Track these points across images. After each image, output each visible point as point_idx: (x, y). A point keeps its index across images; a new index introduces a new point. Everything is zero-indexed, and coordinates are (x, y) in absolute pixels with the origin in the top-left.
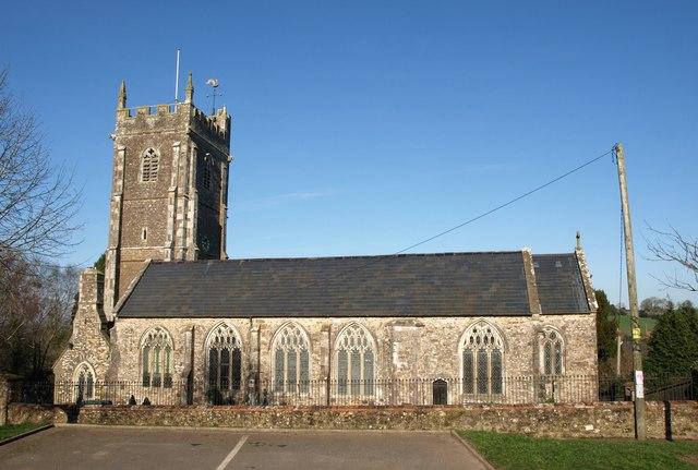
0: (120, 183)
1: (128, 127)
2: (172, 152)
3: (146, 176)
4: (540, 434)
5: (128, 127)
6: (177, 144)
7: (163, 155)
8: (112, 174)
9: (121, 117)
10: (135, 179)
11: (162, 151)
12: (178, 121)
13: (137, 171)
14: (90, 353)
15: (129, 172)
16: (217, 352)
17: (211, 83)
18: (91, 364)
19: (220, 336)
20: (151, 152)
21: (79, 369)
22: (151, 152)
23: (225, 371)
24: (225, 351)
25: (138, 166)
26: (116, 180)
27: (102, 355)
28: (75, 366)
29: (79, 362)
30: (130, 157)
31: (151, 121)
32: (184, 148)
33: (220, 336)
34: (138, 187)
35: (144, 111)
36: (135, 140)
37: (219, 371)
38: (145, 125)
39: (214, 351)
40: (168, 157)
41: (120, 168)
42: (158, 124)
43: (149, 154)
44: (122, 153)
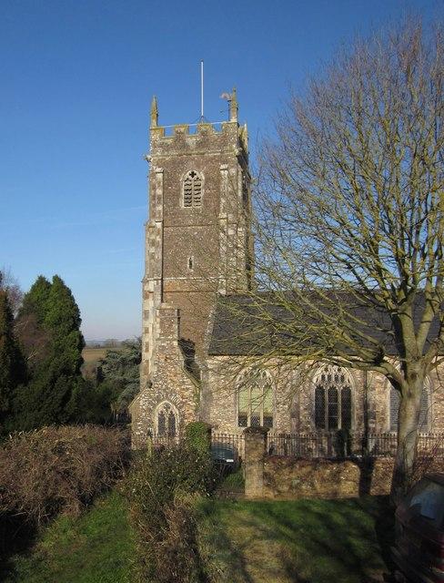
0: (160, 208)
1: (165, 147)
2: (220, 175)
3: (188, 201)
4: (21, 305)
5: (165, 147)
6: (223, 167)
7: (207, 180)
8: (148, 198)
9: (155, 136)
10: (176, 204)
11: (206, 174)
12: (224, 141)
13: (178, 196)
14: (173, 391)
15: (170, 196)
16: (323, 391)
17: (225, 97)
18: (175, 404)
19: (326, 374)
20: (193, 175)
21: (160, 407)
22: (193, 175)
23: (333, 410)
24: (333, 392)
25: (179, 190)
26: (154, 206)
27: (187, 393)
28: (154, 406)
29: (159, 400)
30: (170, 181)
31: (191, 141)
32: (233, 171)
33: (326, 374)
34: (182, 213)
35: (182, 130)
36: (173, 162)
37: (327, 410)
38: (185, 146)
39: (320, 390)
40: (214, 181)
41: (159, 192)
42: (200, 145)
43: (190, 177)
44: (160, 176)
